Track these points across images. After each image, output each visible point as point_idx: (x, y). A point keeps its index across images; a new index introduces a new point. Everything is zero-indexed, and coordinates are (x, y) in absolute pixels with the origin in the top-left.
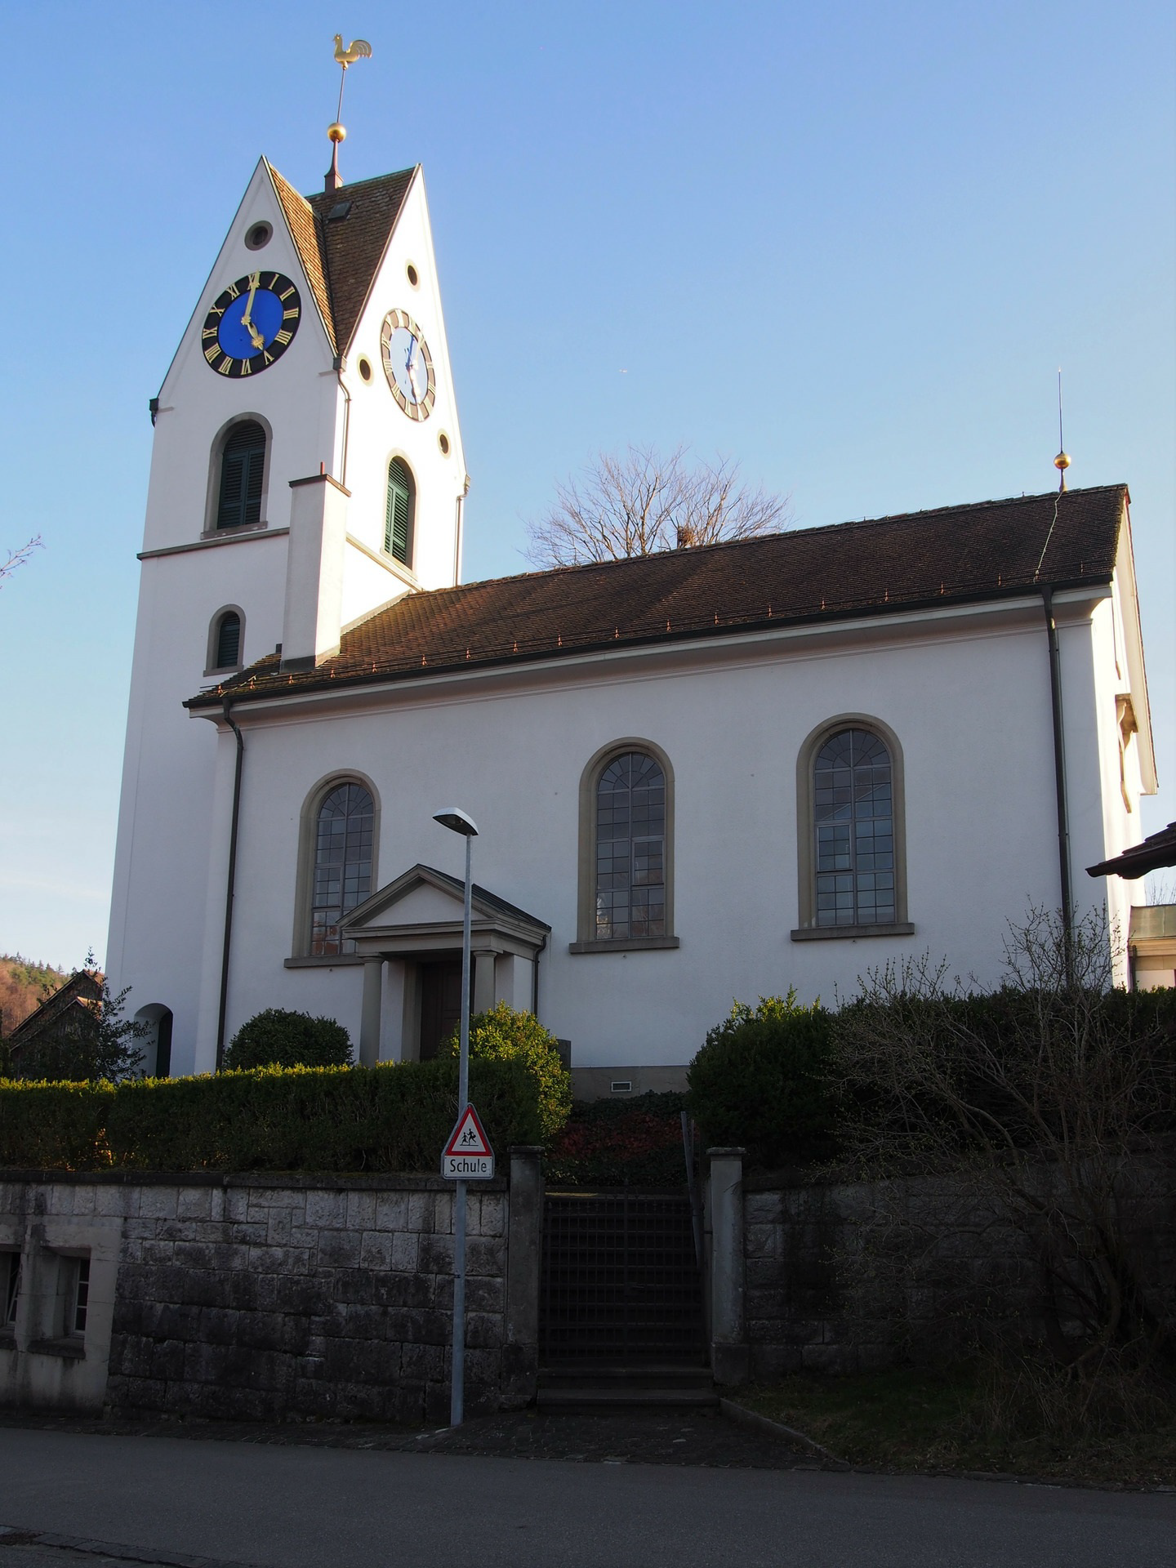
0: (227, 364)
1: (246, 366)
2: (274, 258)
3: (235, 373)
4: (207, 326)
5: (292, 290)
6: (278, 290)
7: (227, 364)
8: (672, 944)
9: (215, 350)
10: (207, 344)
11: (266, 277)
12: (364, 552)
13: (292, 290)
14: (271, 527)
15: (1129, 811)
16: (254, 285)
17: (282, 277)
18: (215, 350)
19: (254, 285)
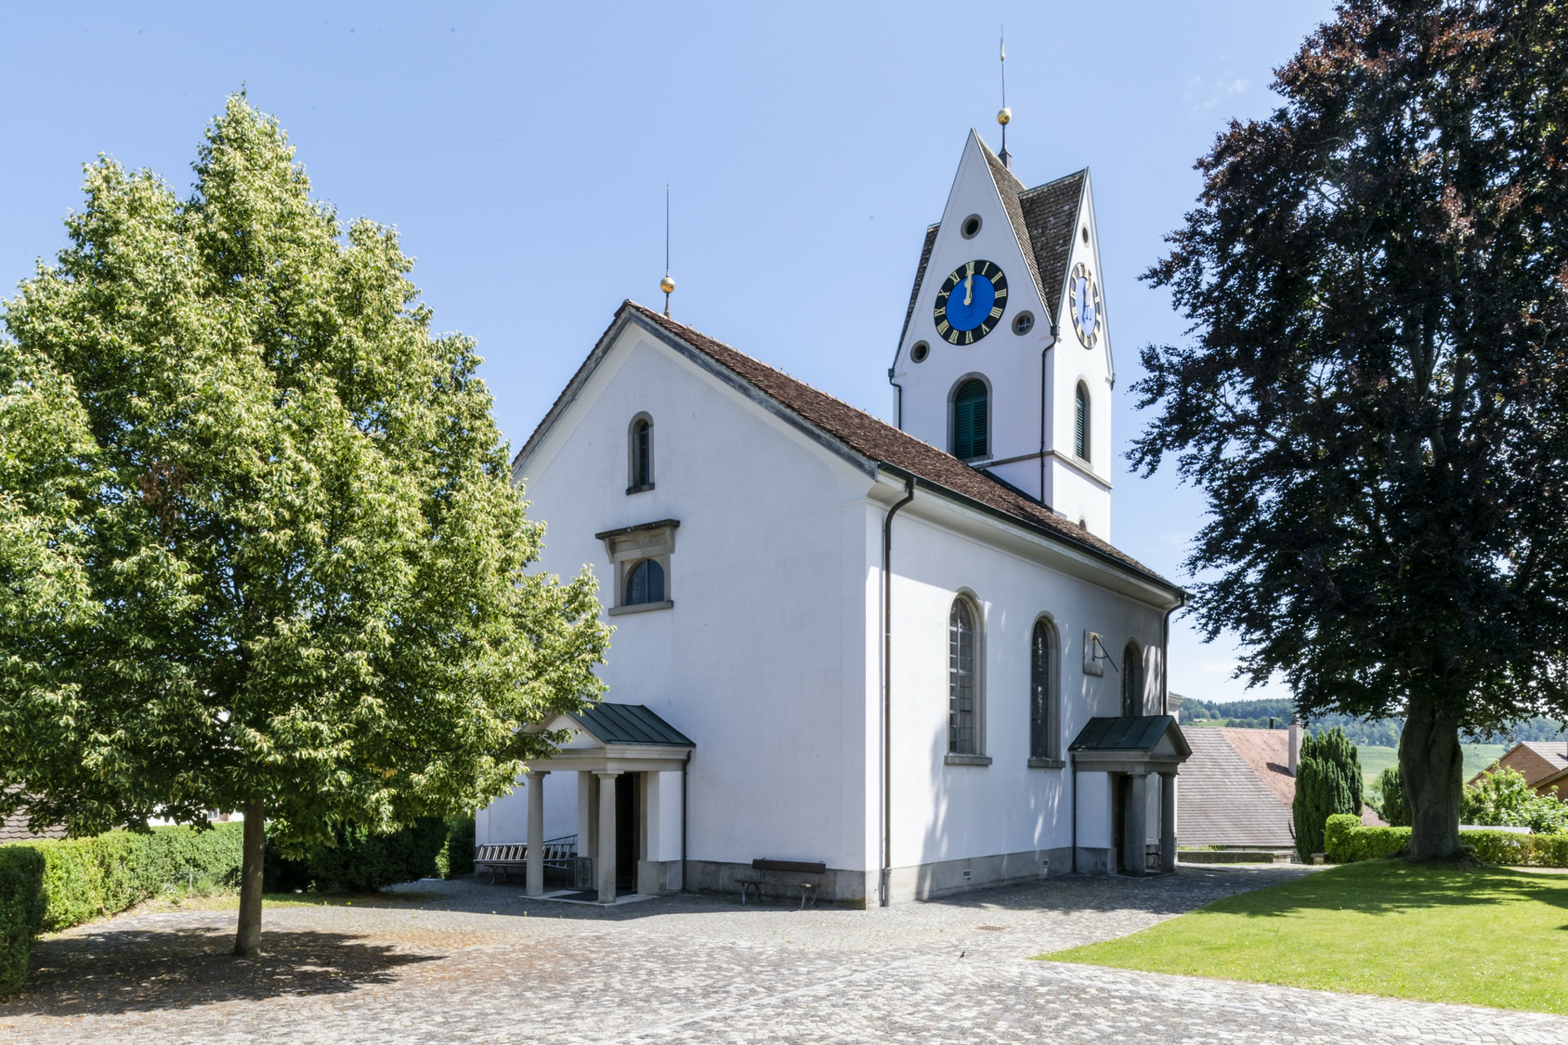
0: (955, 335)
1: (969, 336)
2: (980, 248)
3: (961, 341)
4: (938, 306)
5: (1000, 275)
6: (989, 275)
7: (955, 335)
8: (671, 604)
9: (945, 325)
10: (938, 321)
11: (979, 264)
12: (888, 638)
13: (1000, 275)
14: (995, 459)
15: (641, 429)
16: (970, 273)
17: (992, 265)
18: (945, 325)
19: (970, 273)
